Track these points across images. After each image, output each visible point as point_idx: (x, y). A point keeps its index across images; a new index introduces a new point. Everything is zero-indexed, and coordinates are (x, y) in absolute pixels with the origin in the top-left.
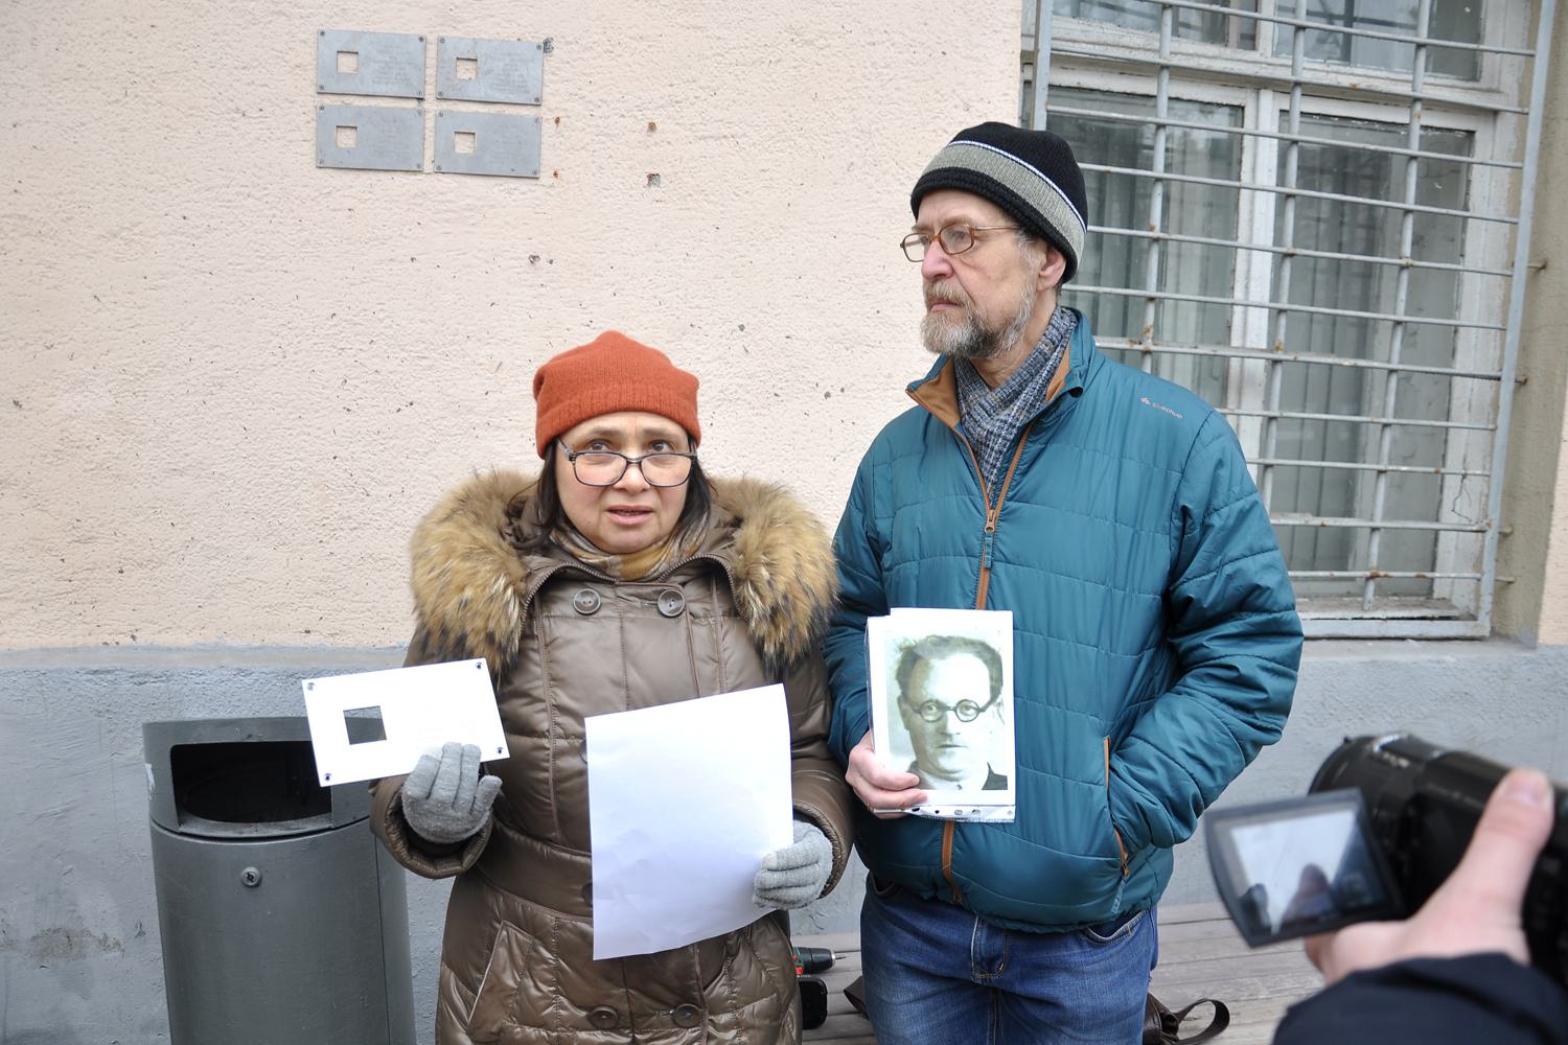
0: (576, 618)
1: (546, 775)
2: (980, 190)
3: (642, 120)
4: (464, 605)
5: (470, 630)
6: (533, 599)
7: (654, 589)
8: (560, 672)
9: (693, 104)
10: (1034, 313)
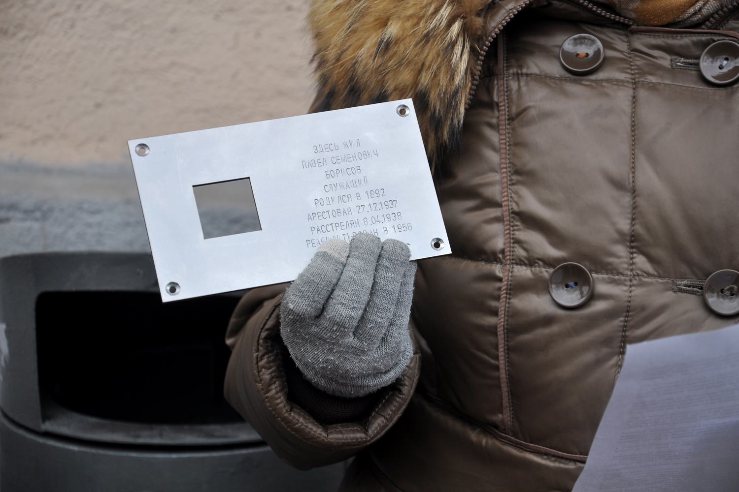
0: (566, 80)
1: (490, 320)
4: (385, 47)
5: (392, 87)
6: (495, 40)
7: (695, 38)
8: (530, 161)
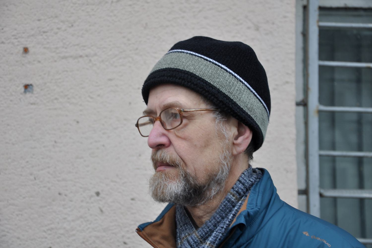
2: (186, 83)
3: (18, 45)
9: (56, 33)
10: (231, 171)
